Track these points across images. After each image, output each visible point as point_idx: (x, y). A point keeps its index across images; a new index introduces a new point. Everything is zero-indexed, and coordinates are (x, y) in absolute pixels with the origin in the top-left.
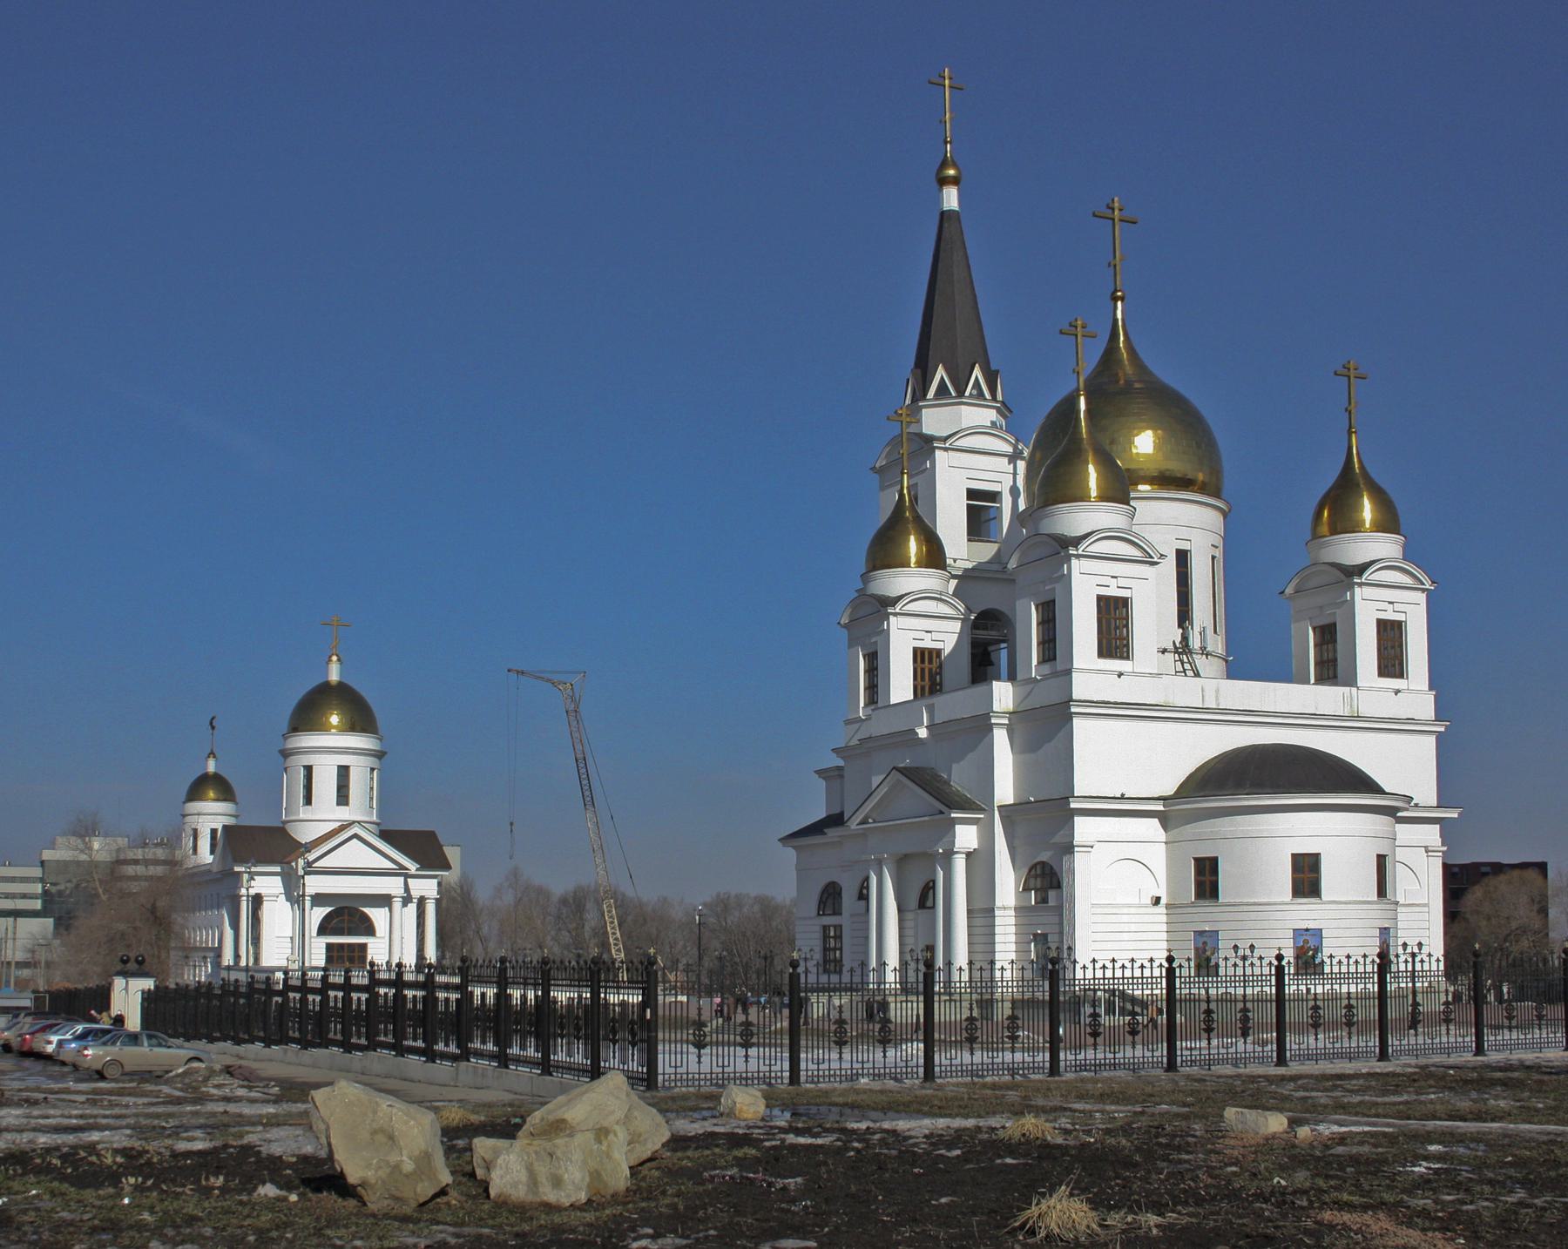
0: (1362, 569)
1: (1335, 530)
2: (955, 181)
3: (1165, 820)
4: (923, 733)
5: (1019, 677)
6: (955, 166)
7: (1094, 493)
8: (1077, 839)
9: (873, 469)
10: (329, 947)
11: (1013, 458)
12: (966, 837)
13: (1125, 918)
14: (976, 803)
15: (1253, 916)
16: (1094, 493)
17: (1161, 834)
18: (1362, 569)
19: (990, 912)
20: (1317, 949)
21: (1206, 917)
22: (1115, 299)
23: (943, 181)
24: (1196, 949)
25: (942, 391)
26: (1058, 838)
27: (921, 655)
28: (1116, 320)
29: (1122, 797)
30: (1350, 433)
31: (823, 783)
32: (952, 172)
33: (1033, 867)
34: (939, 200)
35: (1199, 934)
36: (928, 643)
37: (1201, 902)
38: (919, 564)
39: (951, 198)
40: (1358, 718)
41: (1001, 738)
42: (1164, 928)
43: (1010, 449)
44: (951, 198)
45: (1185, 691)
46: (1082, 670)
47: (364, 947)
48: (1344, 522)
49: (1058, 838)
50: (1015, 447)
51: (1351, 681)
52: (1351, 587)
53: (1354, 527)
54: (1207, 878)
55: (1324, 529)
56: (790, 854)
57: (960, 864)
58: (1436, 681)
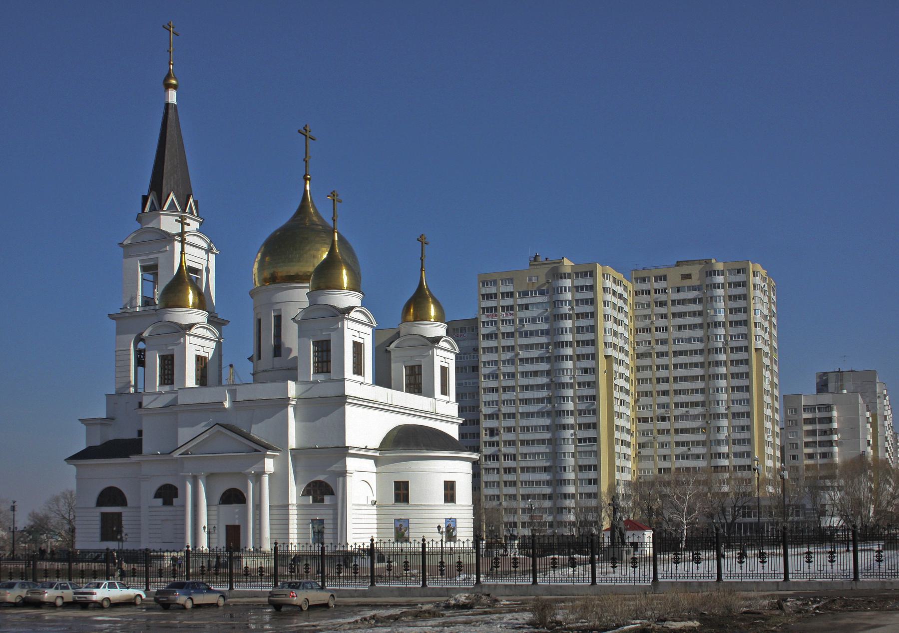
0: (190, 326)
1: (416, 319)
2: (175, 87)
3: (377, 460)
4: (227, 405)
5: (300, 379)
6: (175, 78)
7: (345, 285)
8: (348, 468)
9: (121, 244)
10: (104, 515)
11: (208, 251)
12: (270, 465)
13: (363, 512)
14: (278, 445)
15: (430, 512)
16: (345, 285)
17: (374, 469)
18: (190, 326)
19: (286, 507)
20: (454, 529)
21: (401, 511)
22: (306, 179)
23: (168, 86)
24: (396, 528)
25: (172, 207)
26: (335, 467)
27: (198, 358)
28: (305, 191)
29: (366, 448)
30: (422, 270)
31: (84, 427)
32: (174, 82)
33: (309, 485)
34: (166, 96)
35: (397, 520)
36: (201, 354)
37: (399, 504)
38: (194, 306)
39: (172, 97)
40: (435, 413)
41: (291, 410)
42: (375, 517)
43: (206, 246)
44: (172, 97)
45: (381, 394)
46: (350, 380)
47: (120, 514)
48: (422, 316)
49: (335, 467)
50: (209, 245)
51: (431, 394)
52: (184, 336)
53: (183, 305)
54: (402, 492)
55: (411, 317)
56: (72, 469)
57: (266, 479)
58: (458, 398)
